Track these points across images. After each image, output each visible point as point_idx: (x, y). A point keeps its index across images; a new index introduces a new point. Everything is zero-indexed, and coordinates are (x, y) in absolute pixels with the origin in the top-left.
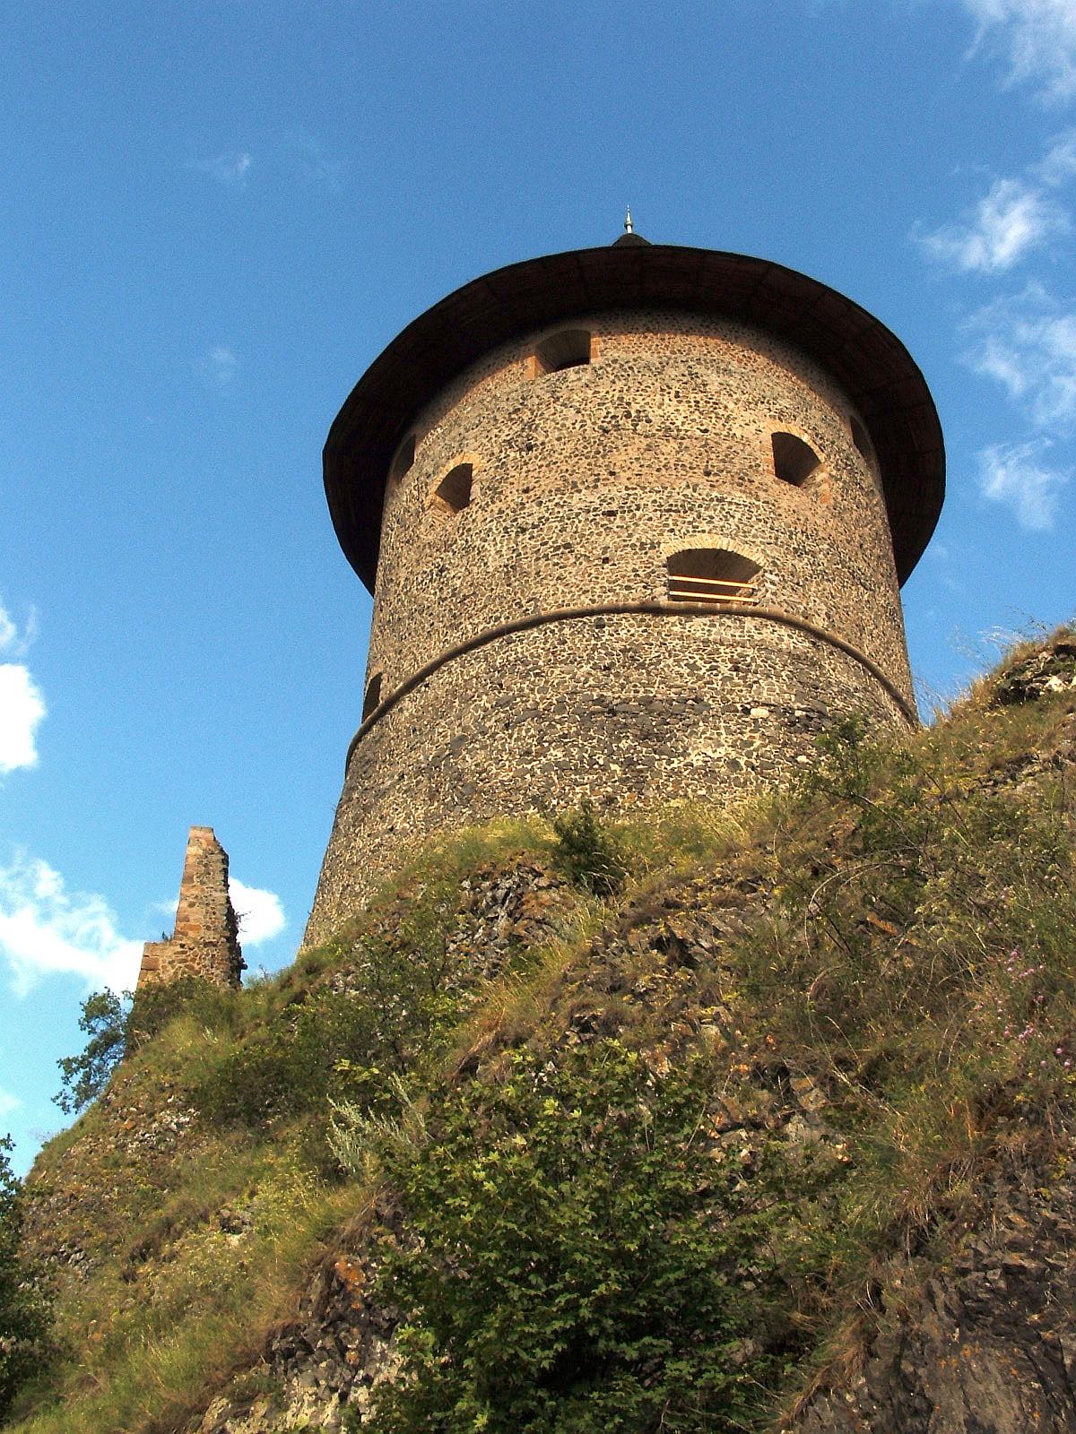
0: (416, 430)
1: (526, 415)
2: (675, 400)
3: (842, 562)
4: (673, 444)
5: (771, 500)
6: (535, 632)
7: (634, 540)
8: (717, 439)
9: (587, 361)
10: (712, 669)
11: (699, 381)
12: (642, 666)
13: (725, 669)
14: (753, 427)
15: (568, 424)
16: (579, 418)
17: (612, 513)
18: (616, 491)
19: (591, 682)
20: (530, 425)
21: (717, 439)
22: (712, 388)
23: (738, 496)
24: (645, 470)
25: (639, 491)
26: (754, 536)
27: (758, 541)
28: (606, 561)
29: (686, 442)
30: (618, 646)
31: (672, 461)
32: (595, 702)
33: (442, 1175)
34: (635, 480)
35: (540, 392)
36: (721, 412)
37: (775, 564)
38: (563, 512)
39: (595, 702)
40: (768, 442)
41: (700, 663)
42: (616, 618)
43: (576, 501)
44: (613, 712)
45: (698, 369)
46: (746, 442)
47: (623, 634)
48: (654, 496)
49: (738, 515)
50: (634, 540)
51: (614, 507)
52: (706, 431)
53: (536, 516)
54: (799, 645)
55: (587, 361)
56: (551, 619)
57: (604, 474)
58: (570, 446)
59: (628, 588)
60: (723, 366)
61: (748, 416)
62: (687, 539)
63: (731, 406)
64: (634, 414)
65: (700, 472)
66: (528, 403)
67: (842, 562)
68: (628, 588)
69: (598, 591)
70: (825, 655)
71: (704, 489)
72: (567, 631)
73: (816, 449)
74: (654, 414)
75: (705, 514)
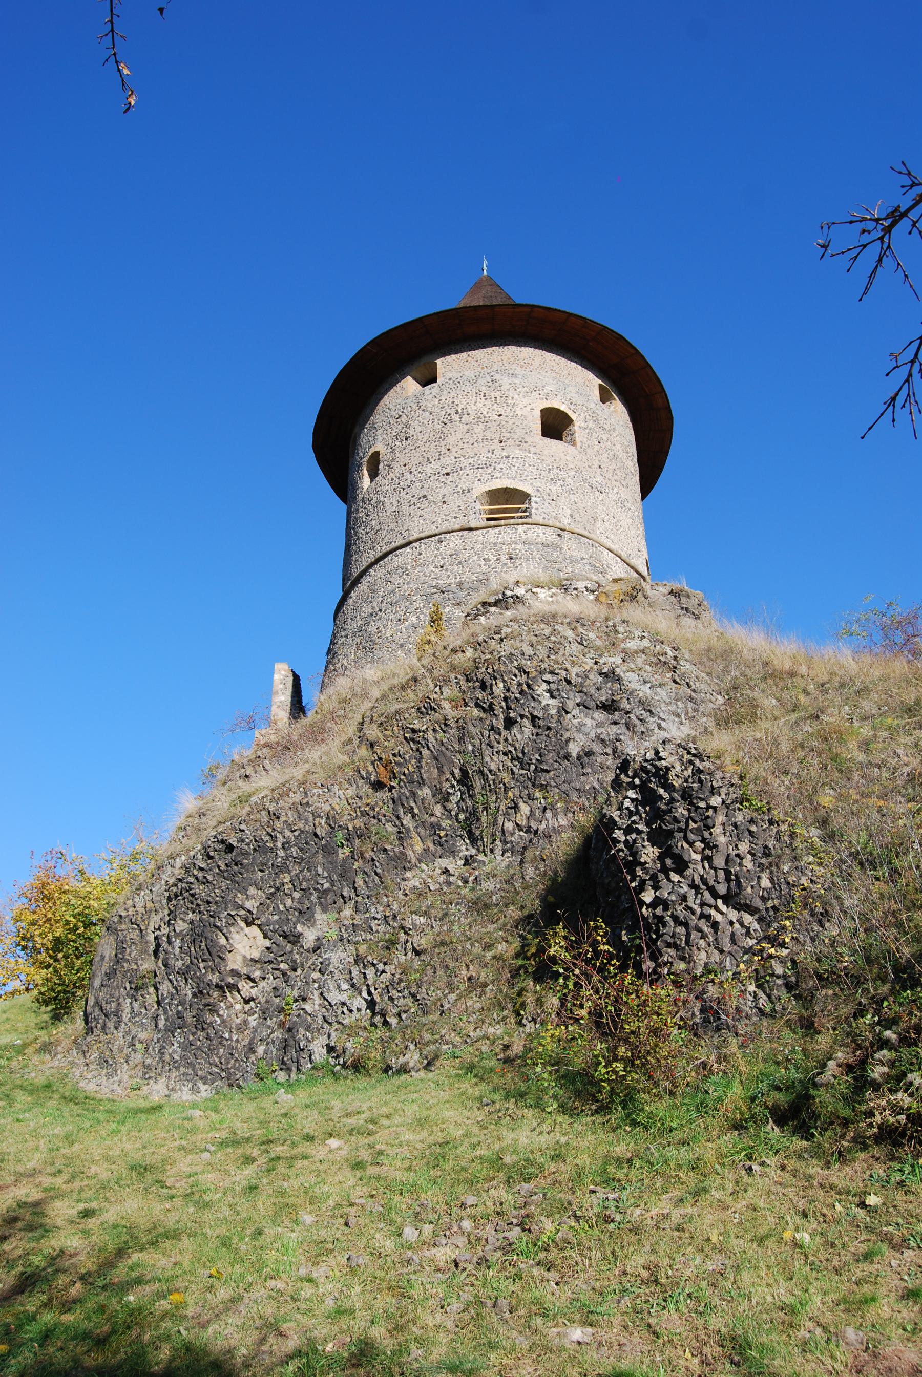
0: (357, 430)
1: (404, 419)
2: (483, 399)
3: (585, 481)
4: (482, 426)
5: (538, 451)
6: (408, 549)
7: (459, 489)
8: (506, 419)
9: (436, 382)
10: (498, 559)
11: (497, 384)
12: (460, 563)
13: (504, 559)
14: (529, 407)
15: (426, 422)
16: (431, 417)
17: (448, 474)
18: (448, 460)
19: (433, 576)
20: (407, 425)
21: (506, 419)
22: (505, 387)
23: (517, 452)
24: (466, 445)
25: (462, 459)
26: (527, 476)
27: (528, 479)
28: (444, 502)
29: (489, 425)
30: (449, 552)
31: (481, 438)
32: (434, 587)
33: (789, 1336)
34: (460, 452)
35: (412, 404)
36: (509, 402)
37: (538, 490)
38: (422, 476)
39: (434, 587)
40: (538, 414)
41: (491, 557)
42: (448, 535)
43: (429, 469)
44: (443, 592)
45: (497, 377)
46: (524, 417)
47: (452, 545)
48: (471, 460)
49: (517, 465)
50: (459, 489)
51: (448, 470)
52: (500, 415)
53: (409, 481)
54: (549, 538)
55: (436, 382)
56: (416, 541)
57: (444, 450)
58: (427, 435)
59: (455, 517)
60: (511, 372)
61: (526, 401)
62: (488, 484)
63: (516, 396)
64: (460, 411)
65: (496, 441)
66: (405, 411)
67: (585, 481)
68: (455, 517)
69: (440, 521)
70: (569, 543)
71: (498, 452)
72: (423, 547)
73: (570, 413)
74: (471, 409)
75: (498, 468)
